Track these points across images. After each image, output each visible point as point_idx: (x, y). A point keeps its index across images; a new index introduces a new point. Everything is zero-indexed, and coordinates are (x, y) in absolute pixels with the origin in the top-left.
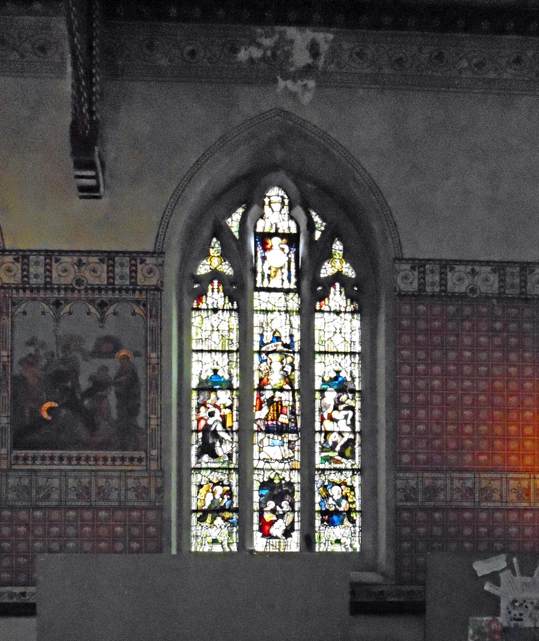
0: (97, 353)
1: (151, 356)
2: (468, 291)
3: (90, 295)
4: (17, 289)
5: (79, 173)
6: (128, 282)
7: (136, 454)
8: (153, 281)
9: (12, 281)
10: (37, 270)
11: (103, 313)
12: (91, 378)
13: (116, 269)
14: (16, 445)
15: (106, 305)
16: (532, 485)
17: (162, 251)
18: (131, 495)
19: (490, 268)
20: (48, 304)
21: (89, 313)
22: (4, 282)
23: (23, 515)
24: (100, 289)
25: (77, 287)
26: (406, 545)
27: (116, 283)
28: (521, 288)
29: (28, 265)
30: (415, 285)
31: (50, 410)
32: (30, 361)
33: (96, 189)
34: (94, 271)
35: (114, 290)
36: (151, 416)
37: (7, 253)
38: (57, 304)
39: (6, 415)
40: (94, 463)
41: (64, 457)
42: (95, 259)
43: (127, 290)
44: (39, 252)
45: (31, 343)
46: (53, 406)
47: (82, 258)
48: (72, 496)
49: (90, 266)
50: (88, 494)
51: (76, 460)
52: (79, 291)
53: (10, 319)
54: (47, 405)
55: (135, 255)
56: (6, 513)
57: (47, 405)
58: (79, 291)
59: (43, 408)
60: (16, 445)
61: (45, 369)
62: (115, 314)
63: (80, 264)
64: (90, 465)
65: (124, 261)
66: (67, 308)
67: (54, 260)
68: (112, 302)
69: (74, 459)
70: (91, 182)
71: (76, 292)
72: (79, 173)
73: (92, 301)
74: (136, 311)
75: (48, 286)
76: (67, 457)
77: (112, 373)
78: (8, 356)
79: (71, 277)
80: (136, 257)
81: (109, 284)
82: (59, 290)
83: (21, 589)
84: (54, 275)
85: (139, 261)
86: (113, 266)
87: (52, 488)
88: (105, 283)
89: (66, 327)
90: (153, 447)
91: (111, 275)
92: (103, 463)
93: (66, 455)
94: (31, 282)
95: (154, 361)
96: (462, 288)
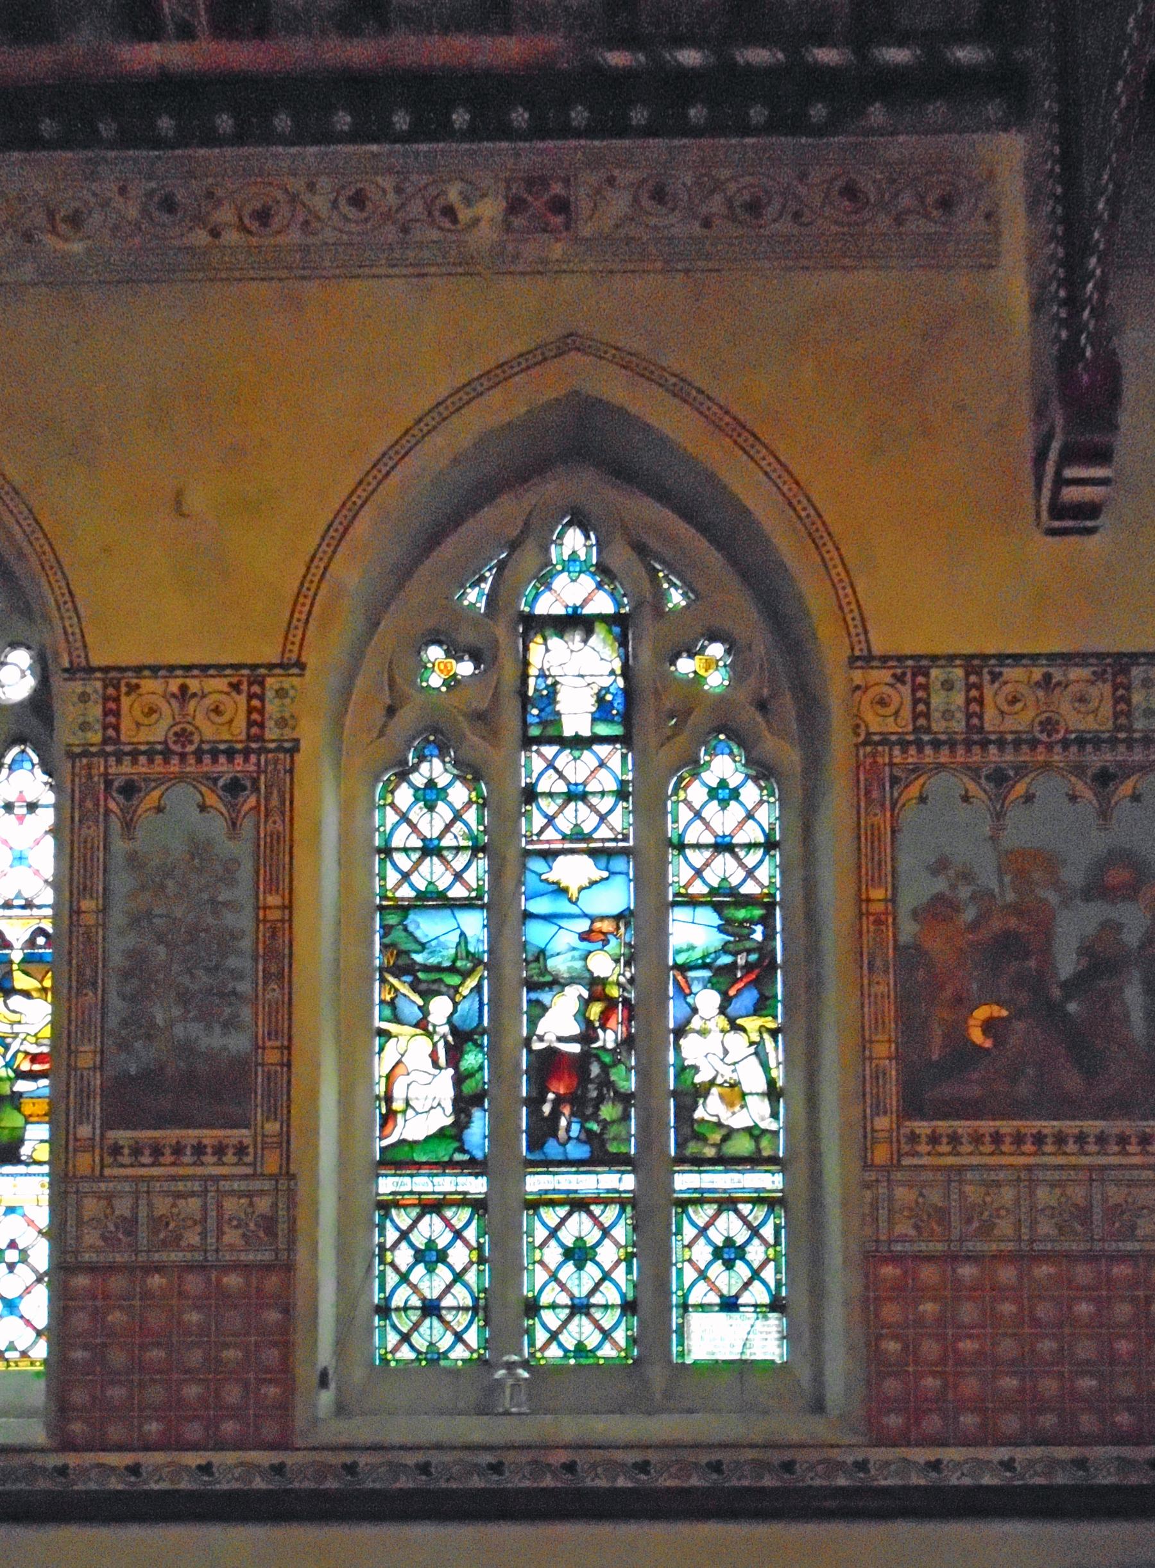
0: (1097, 889)
3: (207, 766)
4: (904, 745)
9: (891, 726)
10: (947, 701)
11: (233, 807)
12: (1085, 950)
13: (269, 707)
14: (913, 1107)
15: (1113, 777)
19: (226, 681)
20: (976, 779)
22: (872, 730)
23: (929, 1273)
25: (177, 748)
27: (268, 735)
28: (105, 728)
29: (1128, 688)
31: (989, 1026)
32: (938, 910)
34: (217, 711)
35: (984, 744)
38: (999, 778)
41: (941, 1136)
42: (1084, 673)
45: (940, 866)
46: (996, 1014)
47: (188, 681)
48: (1045, 1228)
49: (871, 693)
50: (164, 1244)
51: (1054, 1143)
52: (183, 756)
53: (888, 814)
54: (982, 1013)
55: (263, 671)
57: (982, 1013)
58: (183, 756)
59: (971, 1022)
60: (913, 1107)
61: (974, 926)
62: (1136, 798)
65: (89, 690)
66: (1020, 788)
67: (124, 689)
68: (1021, 770)
71: (1041, 748)
73: (1079, 770)
74: (208, 802)
75: (977, 737)
77: (1132, 938)
78: (98, 912)
79: (1031, 713)
81: (1118, 728)
82: (1001, 744)
83: (1003, 1453)
85: (987, 677)
87: (998, 1210)
88: (243, 737)
89: (1023, 829)
93: (1009, 1130)
94: (935, 727)
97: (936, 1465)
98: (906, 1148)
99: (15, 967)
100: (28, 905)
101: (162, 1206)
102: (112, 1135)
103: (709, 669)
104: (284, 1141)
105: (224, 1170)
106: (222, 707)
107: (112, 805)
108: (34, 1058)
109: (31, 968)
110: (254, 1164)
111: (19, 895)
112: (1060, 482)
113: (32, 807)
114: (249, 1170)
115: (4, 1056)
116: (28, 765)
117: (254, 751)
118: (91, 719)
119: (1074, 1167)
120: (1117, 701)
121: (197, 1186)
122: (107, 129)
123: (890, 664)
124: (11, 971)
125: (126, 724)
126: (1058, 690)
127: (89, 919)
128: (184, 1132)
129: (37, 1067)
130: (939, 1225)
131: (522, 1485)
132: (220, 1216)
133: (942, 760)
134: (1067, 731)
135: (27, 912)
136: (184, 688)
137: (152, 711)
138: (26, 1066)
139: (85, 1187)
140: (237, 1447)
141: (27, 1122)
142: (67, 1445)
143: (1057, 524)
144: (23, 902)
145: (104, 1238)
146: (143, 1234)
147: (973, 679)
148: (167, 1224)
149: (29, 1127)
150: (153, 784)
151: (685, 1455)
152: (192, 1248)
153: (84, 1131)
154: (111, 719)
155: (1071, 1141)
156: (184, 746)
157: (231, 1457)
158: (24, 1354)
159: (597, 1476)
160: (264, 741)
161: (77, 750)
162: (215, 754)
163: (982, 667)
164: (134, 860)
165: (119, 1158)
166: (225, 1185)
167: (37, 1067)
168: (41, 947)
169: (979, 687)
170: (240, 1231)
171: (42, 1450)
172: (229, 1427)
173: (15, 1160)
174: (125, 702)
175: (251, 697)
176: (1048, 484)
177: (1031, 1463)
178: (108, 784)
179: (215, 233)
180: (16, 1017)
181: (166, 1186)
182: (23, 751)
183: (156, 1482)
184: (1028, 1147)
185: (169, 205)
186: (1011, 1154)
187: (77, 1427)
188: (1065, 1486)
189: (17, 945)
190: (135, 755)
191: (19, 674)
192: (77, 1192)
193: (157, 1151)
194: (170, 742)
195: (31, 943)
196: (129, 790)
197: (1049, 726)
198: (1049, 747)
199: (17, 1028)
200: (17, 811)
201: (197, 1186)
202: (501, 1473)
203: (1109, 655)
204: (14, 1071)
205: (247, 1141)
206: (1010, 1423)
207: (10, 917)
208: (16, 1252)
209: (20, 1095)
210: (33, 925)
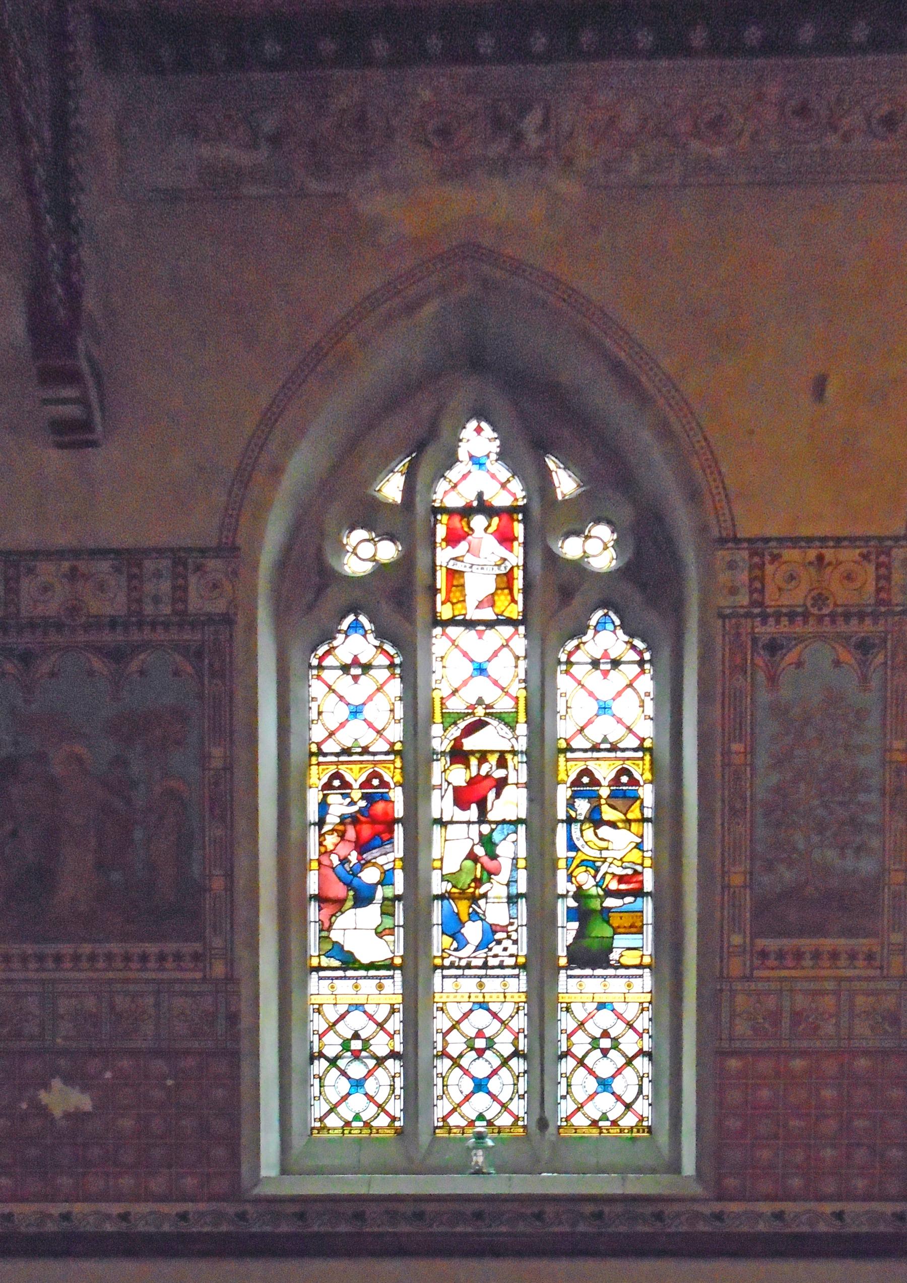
2: (809, 603)
5: (50, 394)
6: (168, 610)
8: (219, 606)
9: (109, 610)
11: (863, 664)
16: (787, 1004)
17: (233, 543)
18: (862, 1028)
19: (858, 551)
21: (176, 673)
25: (815, 611)
26: (734, 1124)
28: (751, 593)
33: (86, 425)
36: (214, 872)
37: (846, 543)
40: (848, 962)
43: (166, 626)
44: (160, 551)
47: (824, 551)
49: (842, 568)
53: (749, 680)
55: (889, 543)
63: (73, 575)
67: (768, 558)
70: (72, 411)
72: (50, 394)
73: (845, 639)
76: (846, 953)
80: (182, 560)
82: (778, 616)
83: (64, 1207)
85: (768, 558)
88: (872, 601)
91: (882, 583)
95: (737, 760)
96: (53, 607)
97: (183, 1216)
98: (757, 962)
99: (603, 801)
100: (614, 748)
101: (801, 1002)
102: (761, 943)
103: (596, 549)
105: (856, 972)
106: (854, 575)
107: (759, 661)
108: (621, 879)
109: (618, 803)
110: (881, 968)
111: (605, 740)
113: (616, 663)
115: (595, 877)
116: (610, 627)
117: (881, 614)
118: (739, 584)
120: (131, 589)
122: (645, 38)
123: (858, 543)
124: (600, 805)
125: (770, 588)
126: (830, 568)
128: (822, 941)
129: (623, 887)
134: (836, 605)
135: (612, 755)
136: (820, 558)
138: (614, 885)
139: (738, 986)
141: (615, 934)
144: (608, 746)
145: (754, 1029)
146: (786, 1023)
147: (756, 559)
149: (616, 937)
150: (794, 643)
152: (32, 1038)
153: (736, 939)
154: (179, 594)
156: (820, 609)
158: (614, 1123)
159: (681, 1223)
160: (891, 605)
161: (728, 611)
162: (847, 616)
163: (764, 549)
164: (779, 710)
166: (857, 985)
167: (623, 887)
168: (625, 785)
169: (762, 567)
171: (694, 1199)
173: (607, 965)
174: (769, 569)
175: (878, 566)
178: (755, 640)
179: (846, 138)
180: (603, 844)
181: (806, 985)
182: (606, 615)
184: (789, 962)
185: (803, 111)
187: (731, 1182)
188: (826, 1234)
189: (605, 783)
190: (32, 625)
191: (601, 546)
193: (24, 959)
194: (809, 605)
195: (616, 781)
196: (773, 647)
197: (820, 599)
198: (820, 619)
199: (605, 854)
200: (602, 667)
201: (830, 986)
203: (874, 538)
204: (603, 890)
205: (876, 949)
207: (598, 759)
208: (360, 1042)
209: (609, 910)
210: (618, 765)
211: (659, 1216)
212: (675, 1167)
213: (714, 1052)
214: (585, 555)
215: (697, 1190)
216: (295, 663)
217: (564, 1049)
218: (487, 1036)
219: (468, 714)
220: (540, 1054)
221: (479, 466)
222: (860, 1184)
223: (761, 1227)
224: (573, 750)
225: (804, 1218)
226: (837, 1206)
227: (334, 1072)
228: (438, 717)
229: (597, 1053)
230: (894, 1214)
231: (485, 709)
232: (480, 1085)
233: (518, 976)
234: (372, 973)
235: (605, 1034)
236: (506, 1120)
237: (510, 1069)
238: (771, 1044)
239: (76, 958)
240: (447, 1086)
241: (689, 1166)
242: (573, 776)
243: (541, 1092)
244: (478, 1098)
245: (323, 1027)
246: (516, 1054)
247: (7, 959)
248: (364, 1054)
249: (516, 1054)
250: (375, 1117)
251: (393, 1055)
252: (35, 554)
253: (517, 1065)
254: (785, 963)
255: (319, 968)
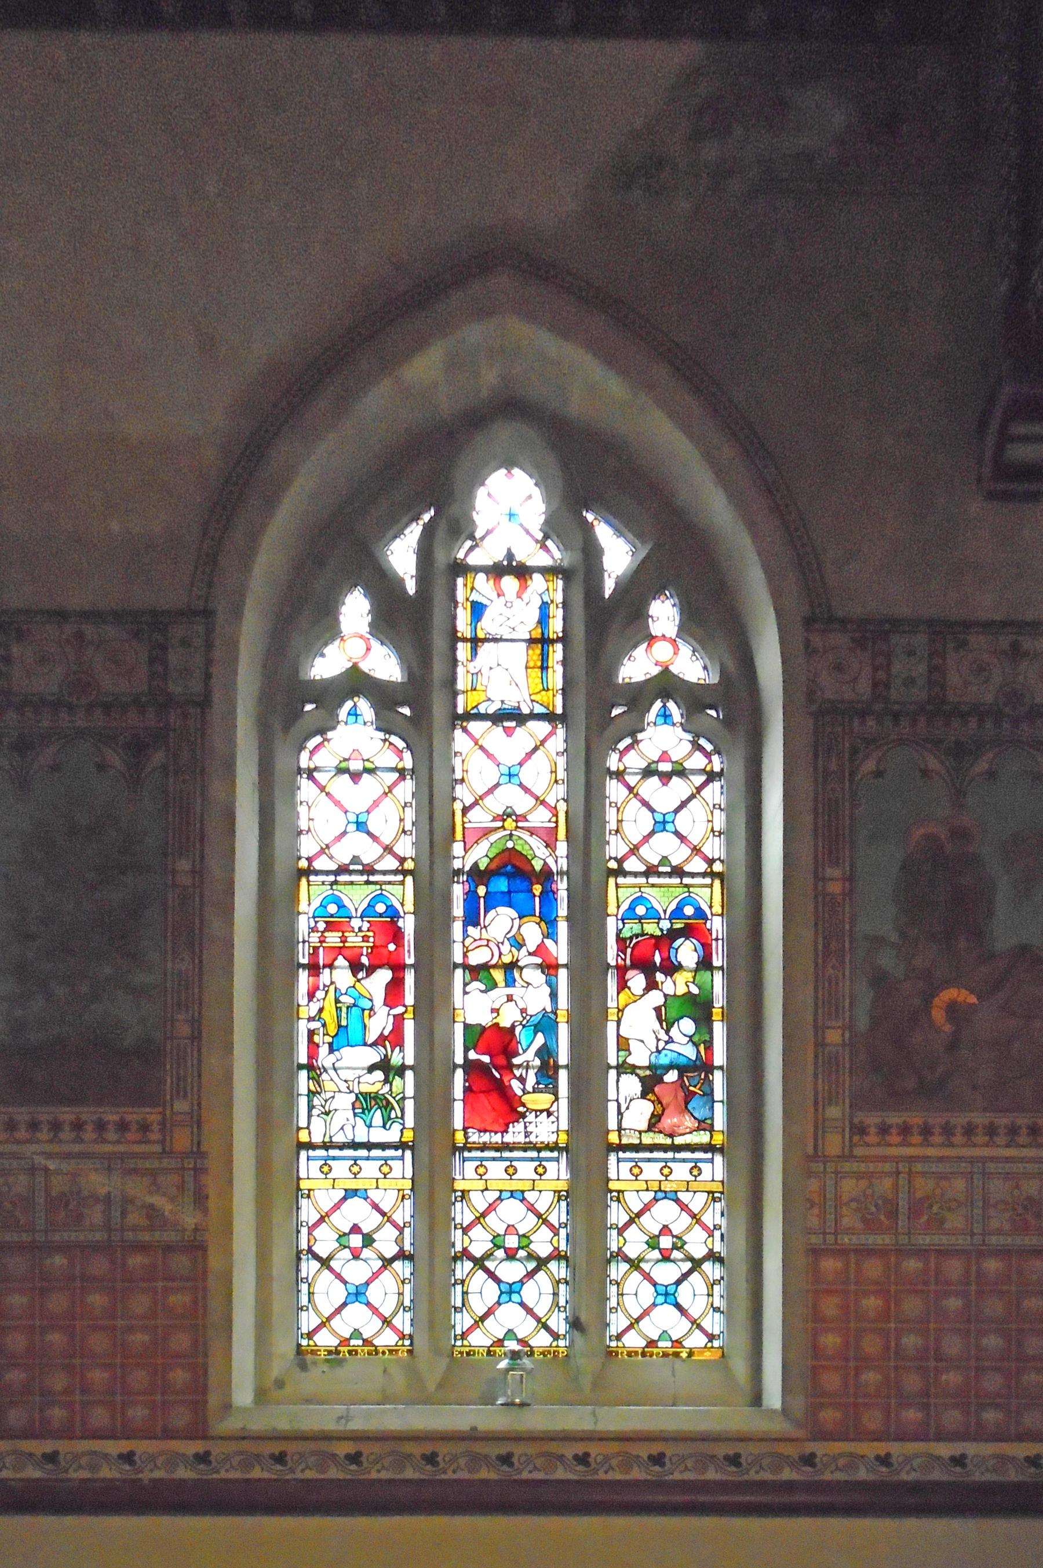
1: (827, 876)
7: (133, 1115)
24: (56, 705)
30: (864, 687)
31: (952, 1009)
39: (840, 1024)
42: (111, 631)
56: (18, 1264)
58: (1016, 722)
64: (868, 1145)
69: (980, 1130)
84: (954, 679)
86: (164, 648)
90: (180, 1092)
91: (881, 675)
92: (94, 1136)
101: (923, 1186)
102: (859, 1117)
104: (196, 1121)
110: (163, 1142)
112: (1005, 438)
114: (157, 1148)
119: (960, 1158)
121: (887, 1167)
127: (835, 888)
130: (888, 1217)
131: (983, 1479)
132: (985, 1201)
133: (79, 723)
137: (981, 669)
140: (916, 1438)
142: (822, 1435)
143: (1001, 486)
148: (67, 1204)
151: (554, 1447)
155: (67, 1128)
157: (988, 1449)
165: (888, 1138)
170: (1007, 1215)
172: (991, 1416)
176: (991, 440)
177: (908, 1459)
183: (75, 1471)
186: (963, 1146)
192: (836, 1173)
202: (662, 1465)
206: (872, 1420)
211: (583, 1459)
212: (757, 1399)
213: (806, 1255)
214: (651, 639)
215: (779, 1427)
216: (282, 762)
217: (459, 1248)
218: (365, 1231)
219: (496, 829)
220: (589, 1263)
221: (509, 506)
222: (57, 1414)
223: (862, 1474)
224: (625, 874)
225: (235, 1461)
226: (881, 1448)
227: (481, 1275)
228: (459, 835)
229: (346, 1254)
230: (1027, 1459)
231: (516, 821)
232: (358, 1294)
233: (557, 1160)
234: (656, 1155)
235: (665, 1230)
236: (697, 1340)
237: (703, 1274)
238: (25, 1237)
239: (884, 1130)
240: (622, 1295)
241: (773, 1395)
242: (316, 903)
243: (433, 1300)
244: (510, 1314)
245: (624, 1218)
246: (401, 1255)
247: (11, 1126)
248: (522, 1253)
249: (401, 1255)
250: (378, 1333)
251: (712, 1256)
252: (967, 625)
253: (402, 1268)
254: (38, 1135)
255: (467, 1147)
